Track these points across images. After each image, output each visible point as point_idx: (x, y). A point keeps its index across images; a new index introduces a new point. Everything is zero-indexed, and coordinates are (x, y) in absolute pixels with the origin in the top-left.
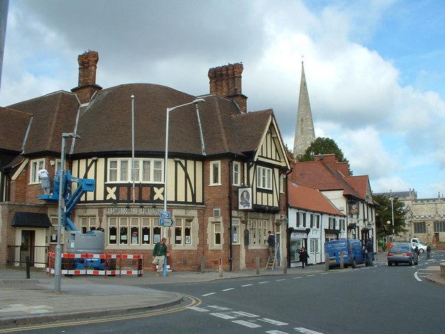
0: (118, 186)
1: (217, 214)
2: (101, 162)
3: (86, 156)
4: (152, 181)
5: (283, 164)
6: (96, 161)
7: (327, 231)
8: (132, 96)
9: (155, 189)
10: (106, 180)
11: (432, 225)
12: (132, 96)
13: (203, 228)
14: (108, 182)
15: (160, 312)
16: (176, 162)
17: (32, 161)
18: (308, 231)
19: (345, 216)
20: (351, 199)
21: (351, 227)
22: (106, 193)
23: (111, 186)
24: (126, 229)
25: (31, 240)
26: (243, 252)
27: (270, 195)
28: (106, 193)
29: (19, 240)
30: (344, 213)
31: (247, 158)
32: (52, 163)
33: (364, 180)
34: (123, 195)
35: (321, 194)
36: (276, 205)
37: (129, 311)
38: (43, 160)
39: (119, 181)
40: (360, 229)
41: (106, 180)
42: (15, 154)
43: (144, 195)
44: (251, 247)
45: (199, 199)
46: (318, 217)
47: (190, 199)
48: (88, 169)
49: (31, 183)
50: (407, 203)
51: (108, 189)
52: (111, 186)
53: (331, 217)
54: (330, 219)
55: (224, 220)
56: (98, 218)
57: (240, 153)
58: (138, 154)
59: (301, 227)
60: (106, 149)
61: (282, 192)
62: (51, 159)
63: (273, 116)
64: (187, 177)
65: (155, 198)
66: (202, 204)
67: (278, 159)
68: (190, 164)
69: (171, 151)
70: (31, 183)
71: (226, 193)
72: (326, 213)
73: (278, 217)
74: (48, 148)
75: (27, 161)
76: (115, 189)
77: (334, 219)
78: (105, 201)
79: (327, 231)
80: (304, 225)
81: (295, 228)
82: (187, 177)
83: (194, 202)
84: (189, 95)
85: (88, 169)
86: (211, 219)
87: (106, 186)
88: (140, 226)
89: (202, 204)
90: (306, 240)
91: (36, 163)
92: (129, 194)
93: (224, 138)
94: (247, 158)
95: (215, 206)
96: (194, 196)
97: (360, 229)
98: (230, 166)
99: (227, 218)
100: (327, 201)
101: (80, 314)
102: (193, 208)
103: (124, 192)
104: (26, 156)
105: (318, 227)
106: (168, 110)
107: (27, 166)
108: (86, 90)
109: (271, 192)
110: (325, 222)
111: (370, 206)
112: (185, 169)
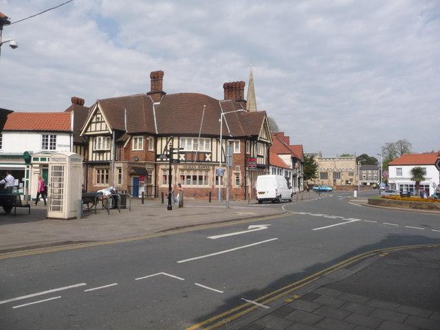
1: (237, 170)
3: (166, 136)
4: (204, 151)
5: (269, 142)
9: (207, 155)
11: (332, 175)
13: (230, 176)
20: (294, 160)
24: (202, 176)
33: (301, 147)
37: (211, 223)
38: (142, 137)
43: (199, 160)
49: (133, 149)
50: (316, 160)
55: (242, 172)
60: (179, 132)
65: (206, 160)
70: (133, 149)
85: (167, 143)
86: (234, 172)
88: (192, 174)
92: (192, 157)
94: (254, 139)
100: (281, 161)
103: (189, 157)
107: (130, 143)
111: (302, 163)
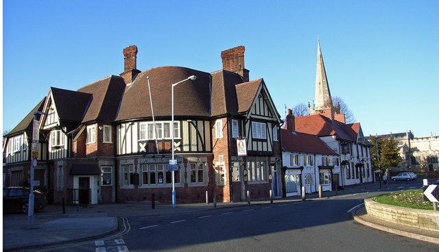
10: (139, 139)
14: (140, 140)
18: (302, 168)
21: (344, 163)
22: (139, 147)
23: (143, 142)
25: (49, 171)
27: (265, 143)
28: (139, 147)
29: (76, 185)
36: (270, 150)
48: (126, 131)
51: (141, 144)
56: (134, 166)
58: (158, 119)
61: (276, 139)
64: (198, 133)
68: (200, 123)
73: (273, 159)
75: (84, 127)
76: (145, 144)
81: (289, 166)
85: (126, 131)
87: (139, 142)
96: (204, 146)
100: (323, 143)
102: (203, 156)
106: (173, 85)
109: (266, 141)
112: (196, 127)
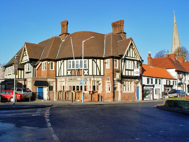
0: (71, 70)
1: (108, 79)
2: (65, 61)
5: (138, 59)
6: (63, 61)
7: (165, 86)
8: (71, 38)
10: (67, 68)
12: (71, 38)
14: (68, 69)
15: (30, 106)
16: (93, 60)
17: (43, 62)
19: (176, 79)
22: (67, 73)
23: (69, 70)
26: (120, 94)
28: (67, 73)
30: (176, 78)
31: (120, 57)
32: (49, 63)
34: (73, 74)
35: (167, 71)
39: (72, 68)
40: (187, 85)
41: (67, 68)
42: (37, 60)
44: (124, 92)
45: (102, 74)
46: (160, 80)
47: (98, 74)
49: (43, 70)
51: (68, 71)
52: (69, 70)
53: (174, 80)
54: (167, 81)
57: (118, 56)
59: (150, 84)
62: (49, 61)
63: (132, 40)
64: (97, 66)
66: (104, 76)
67: (136, 57)
68: (98, 61)
69: (75, 57)
71: (111, 71)
72: (164, 78)
74: (112, 55)
75: (41, 62)
76: (70, 71)
77: (170, 81)
78: (67, 76)
79: (165, 86)
80: (152, 83)
82: (97, 66)
83: (100, 75)
84: (46, 41)
85: (61, 64)
86: (107, 81)
87: (67, 70)
89: (104, 76)
90: (153, 89)
91: (44, 63)
93: (111, 50)
95: (108, 76)
97: (187, 85)
98: (113, 61)
99: (112, 81)
100: (168, 74)
101: (26, 109)
104: (41, 61)
105: (160, 84)
108: (64, 35)
110: (164, 82)
